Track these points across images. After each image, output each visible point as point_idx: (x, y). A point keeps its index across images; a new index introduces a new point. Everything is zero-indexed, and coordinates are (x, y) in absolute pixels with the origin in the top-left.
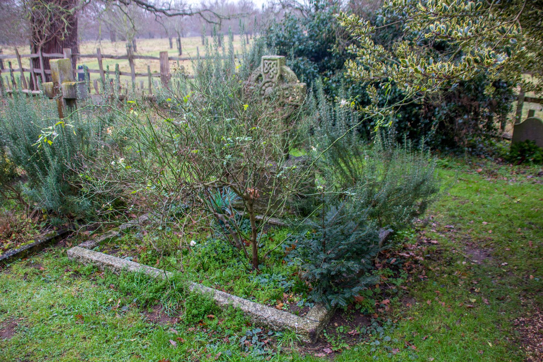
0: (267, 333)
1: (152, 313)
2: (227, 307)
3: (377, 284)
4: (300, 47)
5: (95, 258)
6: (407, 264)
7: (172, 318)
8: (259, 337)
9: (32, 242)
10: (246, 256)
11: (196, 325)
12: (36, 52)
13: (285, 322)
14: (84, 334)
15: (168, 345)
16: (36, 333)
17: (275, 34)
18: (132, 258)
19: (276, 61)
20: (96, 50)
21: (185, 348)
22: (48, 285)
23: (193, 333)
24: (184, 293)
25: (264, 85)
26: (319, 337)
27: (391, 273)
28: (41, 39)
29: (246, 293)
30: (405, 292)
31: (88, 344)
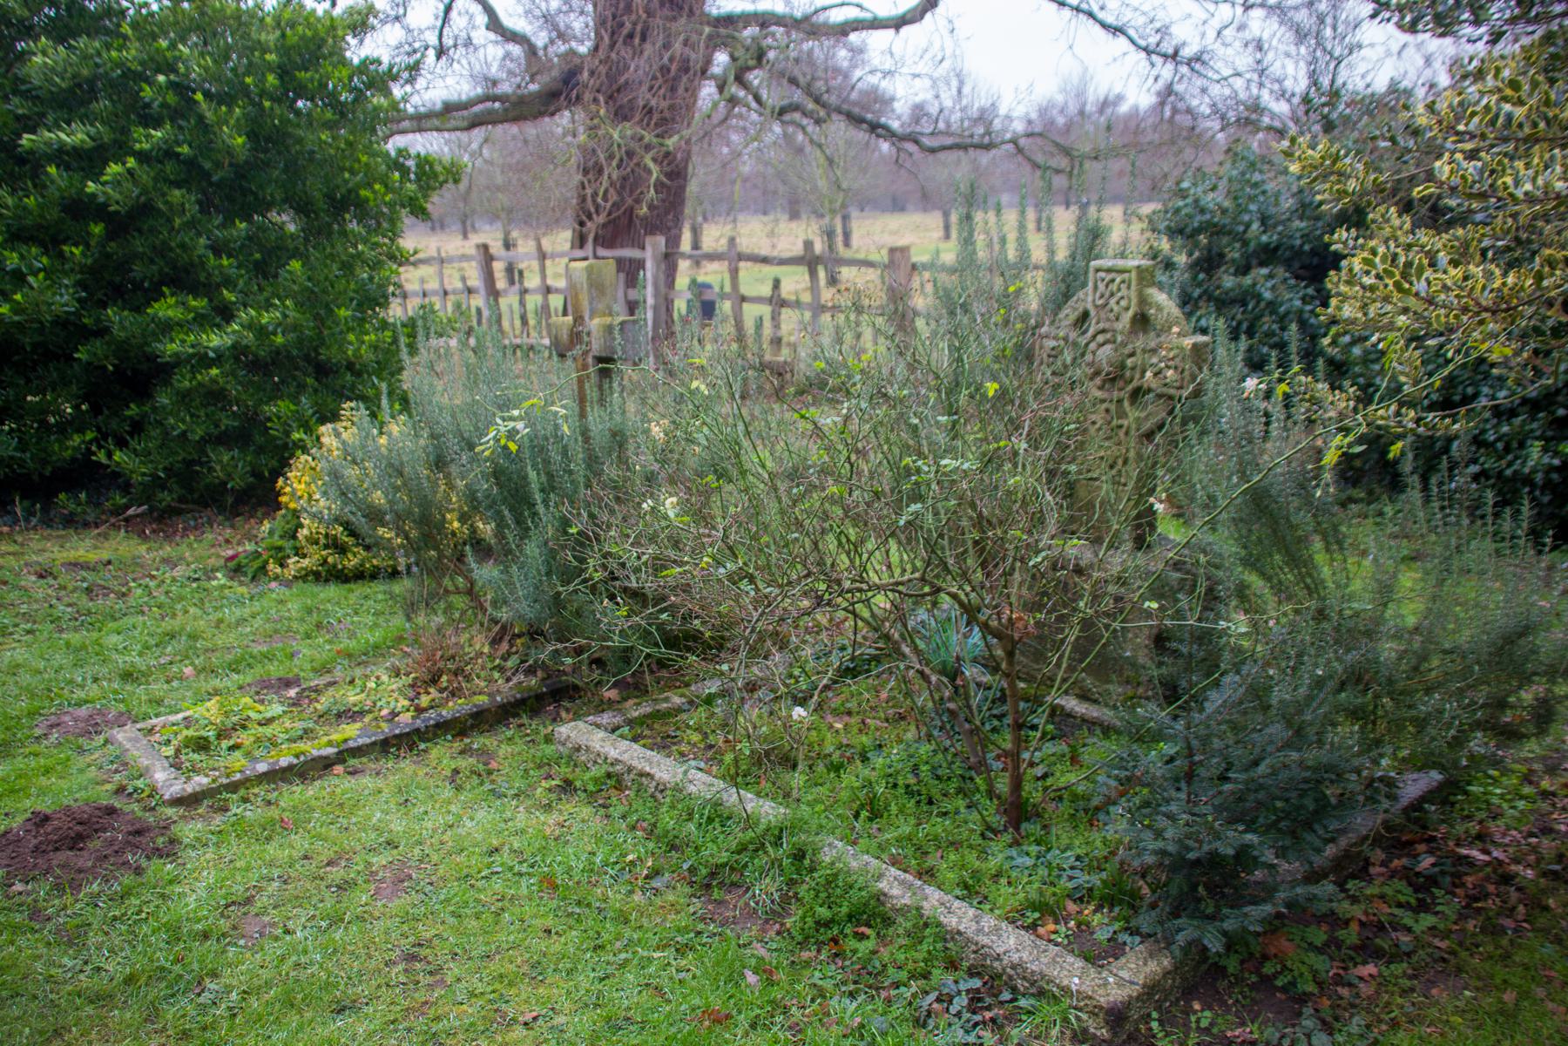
0: (996, 996)
1: (720, 903)
2: (903, 911)
3: (1352, 918)
4: (1264, 238)
5: (613, 754)
6: (1469, 880)
7: (767, 921)
8: (972, 1000)
9: (482, 700)
10: (991, 793)
11: (820, 946)
12: (582, 246)
13: (1046, 971)
14: (549, 922)
15: (735, 978)
16: (447, 900)
17: (1189, 200)
18: (702, 765)
19: (1126, 276)
20: (724, 241)
21: (776, 993)
22: (498, 803)
23: (807, 964)
24: (807, 862)
25: (1094, 337)
26: (1138, 1030)
27: (1408, 895)
28: (597, 212)
29: (966, 887)
30: (1437, 954)
31: (556, 945)
